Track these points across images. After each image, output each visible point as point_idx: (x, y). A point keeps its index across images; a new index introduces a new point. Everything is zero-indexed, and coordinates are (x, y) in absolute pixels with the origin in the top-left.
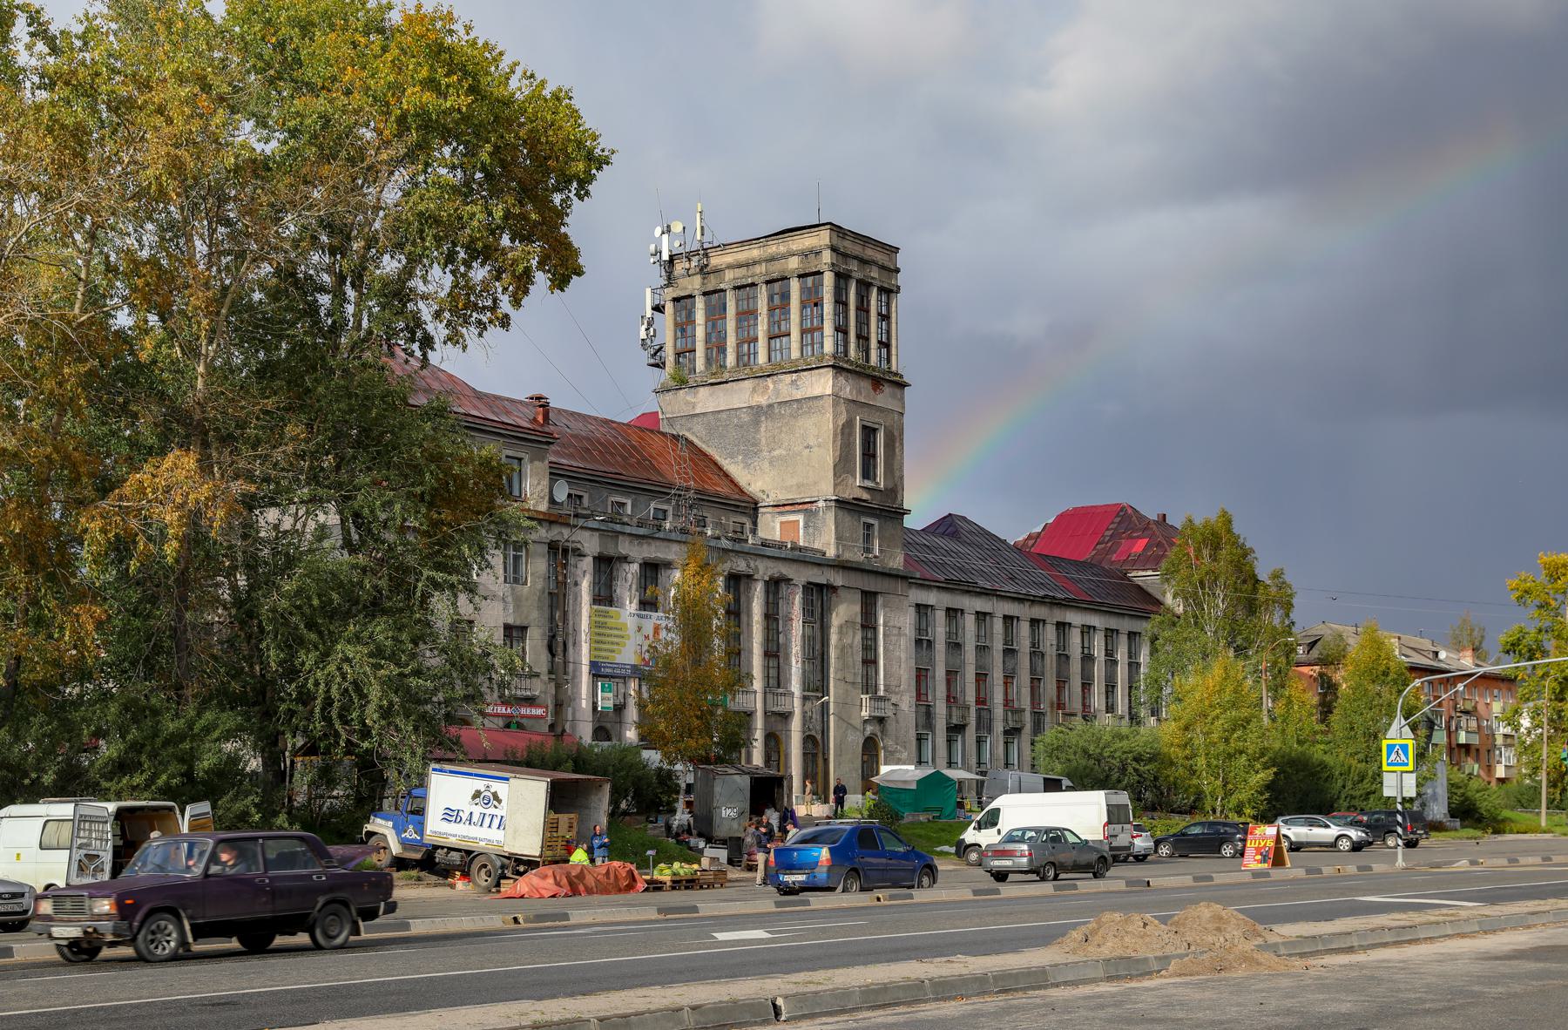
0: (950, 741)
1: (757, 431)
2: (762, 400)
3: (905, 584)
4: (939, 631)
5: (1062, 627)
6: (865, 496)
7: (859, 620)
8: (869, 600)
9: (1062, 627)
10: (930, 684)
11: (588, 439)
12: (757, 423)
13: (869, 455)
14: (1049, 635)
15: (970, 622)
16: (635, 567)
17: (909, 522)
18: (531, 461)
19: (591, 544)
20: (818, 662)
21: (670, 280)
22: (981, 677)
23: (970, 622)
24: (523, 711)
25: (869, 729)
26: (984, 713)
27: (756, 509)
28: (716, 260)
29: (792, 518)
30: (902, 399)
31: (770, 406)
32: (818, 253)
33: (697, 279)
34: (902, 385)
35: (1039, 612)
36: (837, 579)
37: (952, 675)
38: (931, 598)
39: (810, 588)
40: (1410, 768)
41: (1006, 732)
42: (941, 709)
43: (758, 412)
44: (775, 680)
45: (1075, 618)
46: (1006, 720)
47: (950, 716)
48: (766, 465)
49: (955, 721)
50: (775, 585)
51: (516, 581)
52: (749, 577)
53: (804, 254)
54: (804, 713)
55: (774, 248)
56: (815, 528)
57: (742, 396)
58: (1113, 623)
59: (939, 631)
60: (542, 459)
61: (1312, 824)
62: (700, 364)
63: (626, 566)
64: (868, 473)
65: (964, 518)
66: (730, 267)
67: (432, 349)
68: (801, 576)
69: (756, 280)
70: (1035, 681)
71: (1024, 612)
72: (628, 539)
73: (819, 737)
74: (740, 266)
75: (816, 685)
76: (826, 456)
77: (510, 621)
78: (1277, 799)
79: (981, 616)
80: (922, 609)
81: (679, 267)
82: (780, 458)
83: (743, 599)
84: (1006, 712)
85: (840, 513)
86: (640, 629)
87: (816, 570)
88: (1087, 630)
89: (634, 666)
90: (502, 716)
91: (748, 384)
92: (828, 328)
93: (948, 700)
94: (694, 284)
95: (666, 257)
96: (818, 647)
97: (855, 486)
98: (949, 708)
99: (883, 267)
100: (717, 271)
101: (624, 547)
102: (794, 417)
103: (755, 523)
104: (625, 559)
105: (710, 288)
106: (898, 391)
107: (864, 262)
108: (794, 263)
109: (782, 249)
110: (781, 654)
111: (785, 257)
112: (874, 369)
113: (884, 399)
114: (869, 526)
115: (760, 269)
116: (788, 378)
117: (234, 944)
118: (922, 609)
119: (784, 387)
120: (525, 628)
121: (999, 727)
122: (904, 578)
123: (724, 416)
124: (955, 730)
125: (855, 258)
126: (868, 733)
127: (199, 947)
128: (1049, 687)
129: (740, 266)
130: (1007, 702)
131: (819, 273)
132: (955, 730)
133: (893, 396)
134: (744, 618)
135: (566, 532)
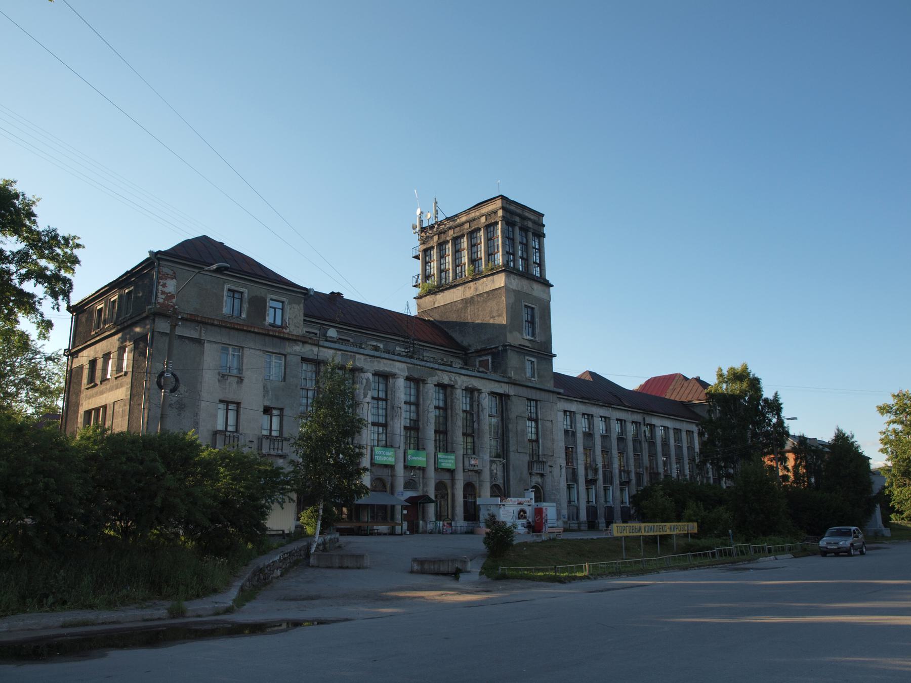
10: (575, 456)
11: (686, 535)
29: (485, 358)
31: (472, 298)
41: (621, 484)
42: (581, 471)
47: (586, 475)
49: (590, 477)
53: (488, 215)
55: (473, 215)
58: (678, 425)
61: (110, 605)
63: (362, 375)
73: (501, 486)
77: (267, 403)
87: (497, 384)
99: (534, 222)
104: (361, 370)
109: (477, 214)
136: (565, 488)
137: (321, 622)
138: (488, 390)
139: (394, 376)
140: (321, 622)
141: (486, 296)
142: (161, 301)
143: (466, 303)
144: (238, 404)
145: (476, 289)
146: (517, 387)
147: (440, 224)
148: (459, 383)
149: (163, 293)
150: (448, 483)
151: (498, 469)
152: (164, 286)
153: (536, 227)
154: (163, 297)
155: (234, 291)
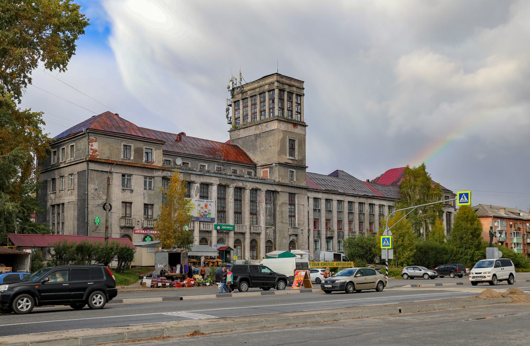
0: (327, 242)
1: (256, 142)
2: (258, 132)
3: (306, 191)
4: (323, 205)
5: (371, 205)
6: (290, 162)
7: (288, 202)
8: (292, 196)
9: (371, 205)
12: (256, 139)
13: (292, 148)
14: (367, 208)
15: (335, 204)
16: (198, 185)
17: (307, 170)
18: (155, 150)
19: (198, 180)
20: (272, 216)
21: (233, 96)
22: (340, 222)
23: (335, 204)
24: (151, 232)
25: (292, 238)
26: (341, 233)
27: (256, 167)
28: (246, 89)
29: (266, 170)
30: (305, 130)
31: (260, 134)
32: (273, 83)
33: (240, 95)
34: (305, 126)
35: (362, 200)
36: (279, 189)
37: (328, 221)
38: (319, 195)
39: (268, 192)
40: (390, 247)
43: (257, 136)
44: (255, 221)
45: (377, 202)
46: (349, 235)
47: (326, 234)
48: (259, 153)
49: (328, 236)
50: (254, 191)
51: (150, 189)
52: (244, 188)
54: (266, 233)
55: (261, 83)
56: (273, 173)
57: (252, 131)
59: (323, 205)
60: (160, 150)
62: (241, 122)
63: (194, 185)
64: (292, 153)
65: (342, 171)
66: (249, 90)
67: (21, 96)
68: (264, 188)
69: (256, 94)
70: (361, 223)
71: (356, 200)
72: (194, 176)
73: (273, 241)
74: (252, 90)
75: (272, 222)
76: (277, 149)
77: (146, 202)
78: (128, 259)
79: (339, 202)
80: (316, 199)
81: (236, 91)
82: (263, 150)
83: (242, 195)
84: (349, 233)
85: (280, 167)
86: (199, 205)
88: (381, 206)
89: (197, 218)
90: (143, 234)
91: (254, 127)
92: (276, 108)
93: (327, 229)
94: (239, 97)
95: (231, 88)
96: (273, 211)
97: (286, 158)
98: (326, 231)
99: (298, 88)
100: (246, 92)
101: (193, 178)
102: (267, 137)
103: (256, 172)
104: (193, 182)
105: (244, 97)
106: (303, 128)
107: (290, 86)
108: (267, 87)
109: (264, 83)
110: (258, 214)
111: (264, 85)
112: (294, 120)
113: (298, 130)
114: (293, 172)
115: (257, 90)
116: (265, 124)
117: (69, 307)
118: (316, 199)
119: (264, 128)
120: (153, 205)
121: (323, 237)
122: (305, 189)
123: (247, 138)
124: (329, 239)
125: (287, 84)
126: (291, 240)
127: (35, 309)
128: (366, 225)
129: (252, 90)
130: (350, 229)
131: (274, 90)
132: (329, 239)
133: (302, 129)
134: (243, 202)
135: (169, 173)
136: (347, 223)
137: (308, 237)
138: (265, 189)
139: (211, 184)
140: (308, 237)
141: (190, 233)
142: (91, 154)
143: (256, 137)
144: (131, 203)
145: (262, 129)
146: (282, 187)
147: (242, 87)
148: (248, 187)
149: (92, 149)
150: (242, 240)
151: (270, 231)
152: (92, 146)
153: (298, 90)
154: (92, 151)
155: (126, 146)
